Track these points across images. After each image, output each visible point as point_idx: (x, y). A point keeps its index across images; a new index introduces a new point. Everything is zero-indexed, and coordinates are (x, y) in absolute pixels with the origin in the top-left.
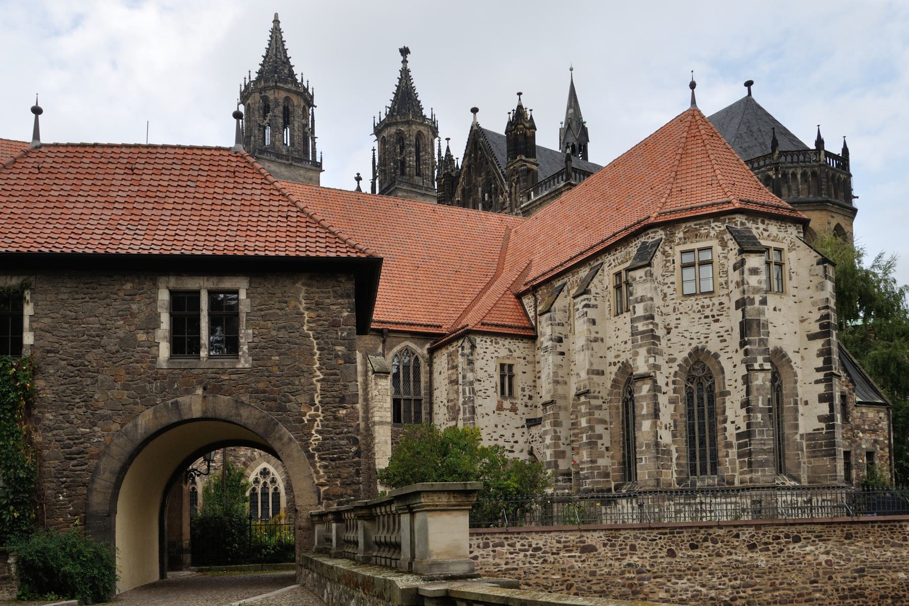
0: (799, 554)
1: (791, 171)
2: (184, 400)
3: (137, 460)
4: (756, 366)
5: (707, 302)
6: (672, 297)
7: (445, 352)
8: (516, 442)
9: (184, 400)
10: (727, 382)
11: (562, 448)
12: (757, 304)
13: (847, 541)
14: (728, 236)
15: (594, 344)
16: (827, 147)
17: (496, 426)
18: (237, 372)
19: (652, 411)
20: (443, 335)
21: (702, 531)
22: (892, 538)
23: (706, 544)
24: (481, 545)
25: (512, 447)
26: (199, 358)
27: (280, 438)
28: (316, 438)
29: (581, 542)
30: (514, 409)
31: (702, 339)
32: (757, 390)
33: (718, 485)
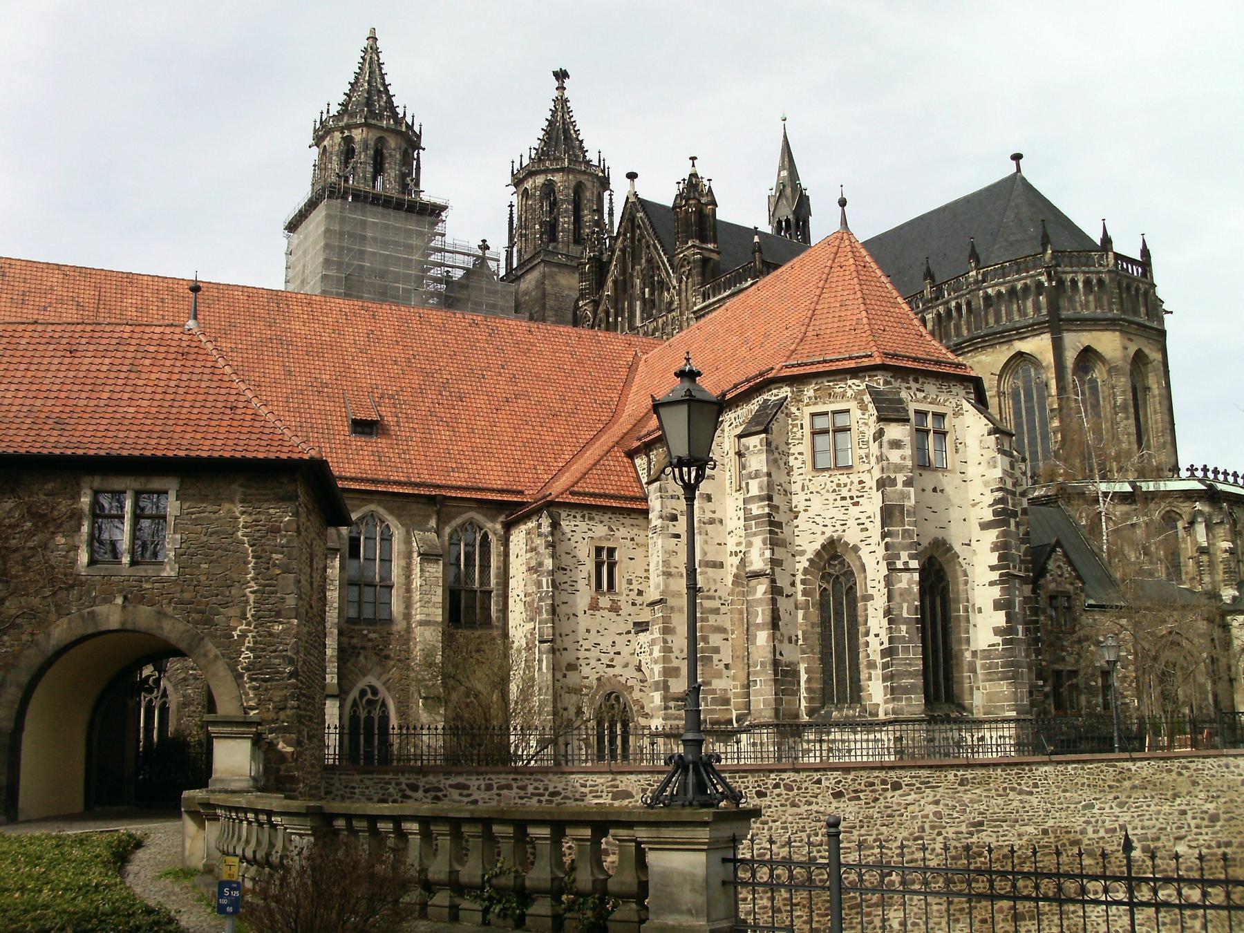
0: (899, 804)
1: (1069, 277)
2: (101, 609)
3: (50, 674)
4: (899, 565)
5: (844, 479)
6: (801, 471)
7: (523, 527)
8: (619, 653)
9: (101, 609)
10: (869, 584)
11: (675, 663)
12: (900, 486)
13: (963, 788)
14: (867, 398)
15: (709, 527)
16: (1118, 247)
17: (588, 631)
18: (162, 581)
19: (768, 619)
20: (521, 504)
21: (773, 776)
22: (1019, 784)
23: (777, 791)
24: (483, 787)
25: (612, 660)
26: (120, 563)
27: (206, 655)
28: (246, 656)
29: (613, 786)
30: (615, 609)
31: (838, 527)
32: (901, 594)
33: (860, 716)
